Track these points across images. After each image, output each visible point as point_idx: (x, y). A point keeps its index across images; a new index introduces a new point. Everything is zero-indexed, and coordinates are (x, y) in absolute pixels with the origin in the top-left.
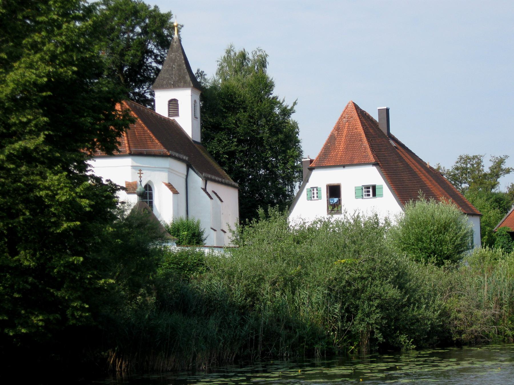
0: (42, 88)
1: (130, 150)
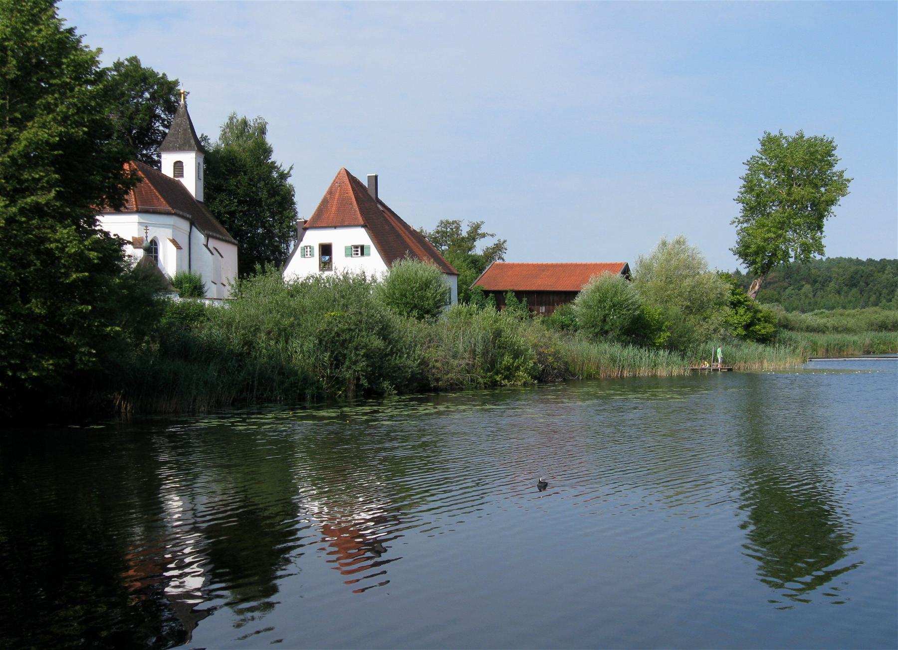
0: (53, 147)
1: (137, 208)
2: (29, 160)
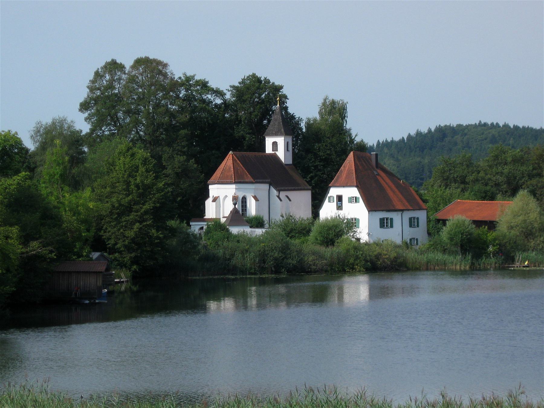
0: (151, 209)
1: (235, 181)
2: (146, 212)
